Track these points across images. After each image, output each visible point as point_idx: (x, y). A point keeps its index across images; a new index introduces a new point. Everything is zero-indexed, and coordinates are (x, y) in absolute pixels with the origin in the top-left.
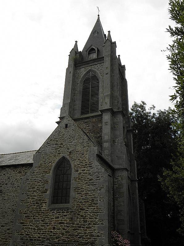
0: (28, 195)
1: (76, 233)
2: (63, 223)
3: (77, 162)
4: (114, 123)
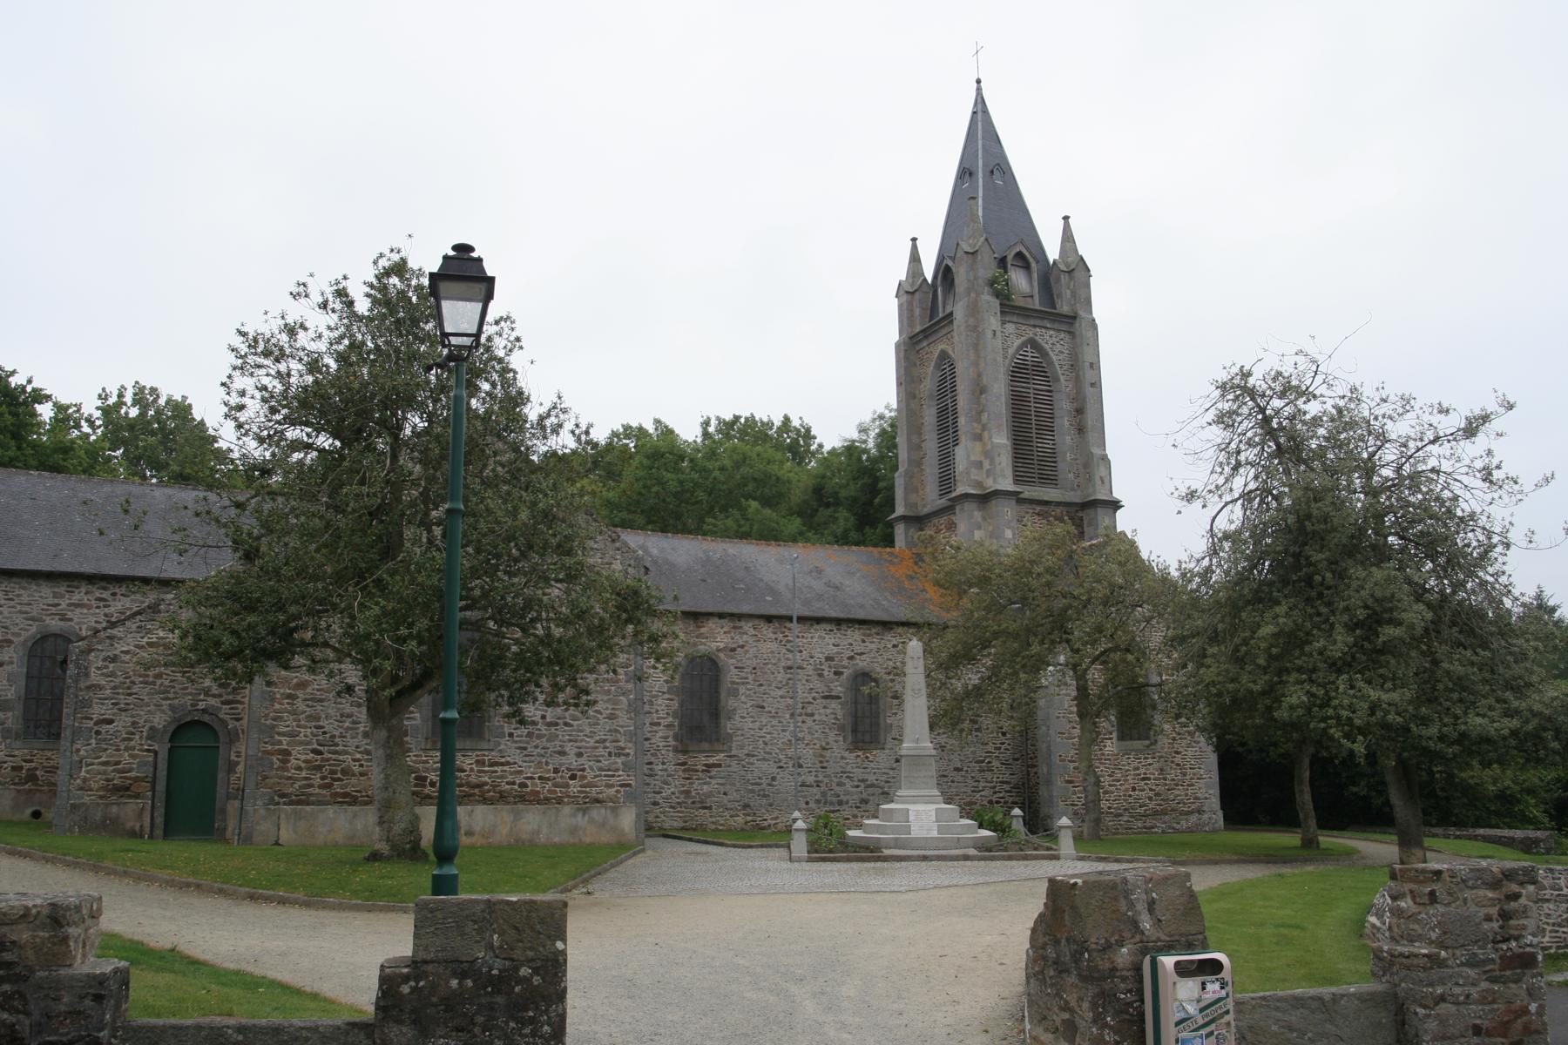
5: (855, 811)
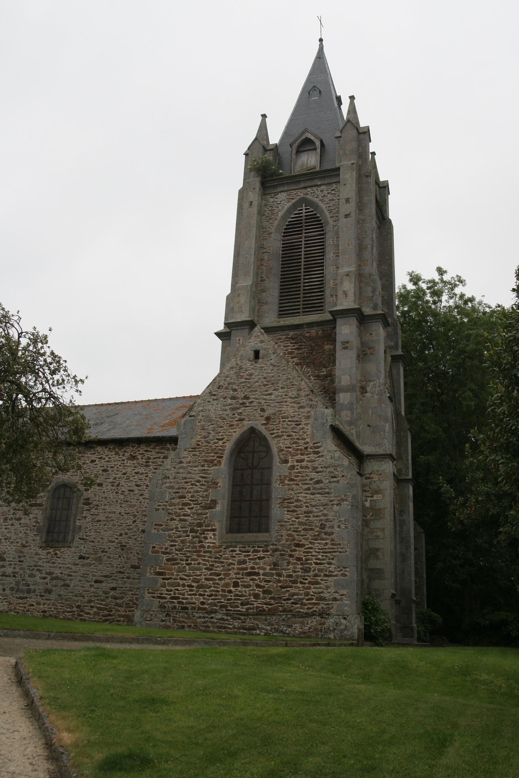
0: (169, 513)
1: (287, 595)
2: (258, 574)
3: (284, 443)
4: (363, 344)
5: (39, 599)
